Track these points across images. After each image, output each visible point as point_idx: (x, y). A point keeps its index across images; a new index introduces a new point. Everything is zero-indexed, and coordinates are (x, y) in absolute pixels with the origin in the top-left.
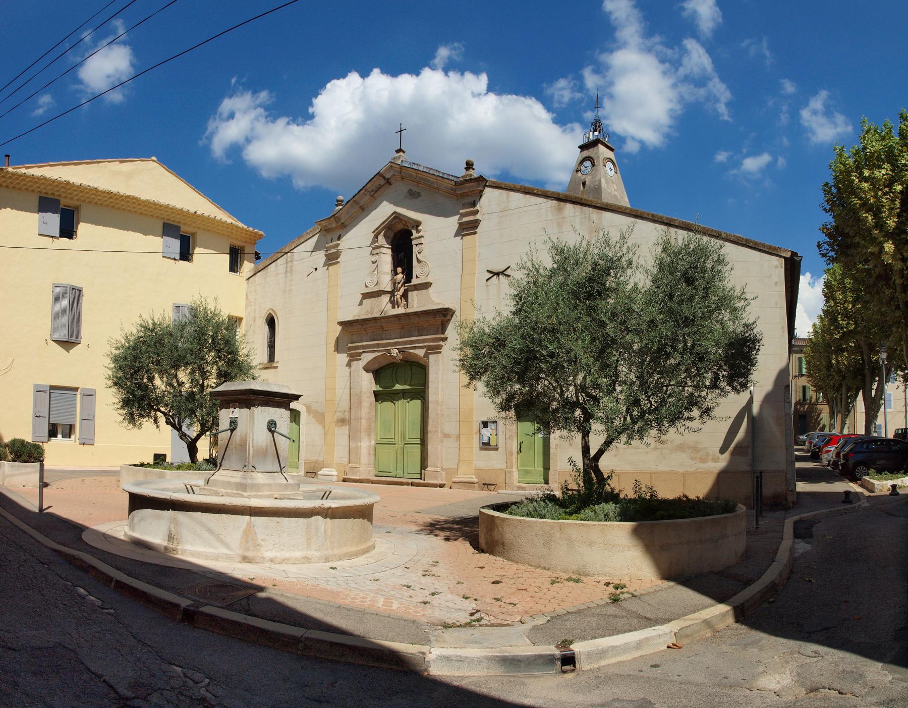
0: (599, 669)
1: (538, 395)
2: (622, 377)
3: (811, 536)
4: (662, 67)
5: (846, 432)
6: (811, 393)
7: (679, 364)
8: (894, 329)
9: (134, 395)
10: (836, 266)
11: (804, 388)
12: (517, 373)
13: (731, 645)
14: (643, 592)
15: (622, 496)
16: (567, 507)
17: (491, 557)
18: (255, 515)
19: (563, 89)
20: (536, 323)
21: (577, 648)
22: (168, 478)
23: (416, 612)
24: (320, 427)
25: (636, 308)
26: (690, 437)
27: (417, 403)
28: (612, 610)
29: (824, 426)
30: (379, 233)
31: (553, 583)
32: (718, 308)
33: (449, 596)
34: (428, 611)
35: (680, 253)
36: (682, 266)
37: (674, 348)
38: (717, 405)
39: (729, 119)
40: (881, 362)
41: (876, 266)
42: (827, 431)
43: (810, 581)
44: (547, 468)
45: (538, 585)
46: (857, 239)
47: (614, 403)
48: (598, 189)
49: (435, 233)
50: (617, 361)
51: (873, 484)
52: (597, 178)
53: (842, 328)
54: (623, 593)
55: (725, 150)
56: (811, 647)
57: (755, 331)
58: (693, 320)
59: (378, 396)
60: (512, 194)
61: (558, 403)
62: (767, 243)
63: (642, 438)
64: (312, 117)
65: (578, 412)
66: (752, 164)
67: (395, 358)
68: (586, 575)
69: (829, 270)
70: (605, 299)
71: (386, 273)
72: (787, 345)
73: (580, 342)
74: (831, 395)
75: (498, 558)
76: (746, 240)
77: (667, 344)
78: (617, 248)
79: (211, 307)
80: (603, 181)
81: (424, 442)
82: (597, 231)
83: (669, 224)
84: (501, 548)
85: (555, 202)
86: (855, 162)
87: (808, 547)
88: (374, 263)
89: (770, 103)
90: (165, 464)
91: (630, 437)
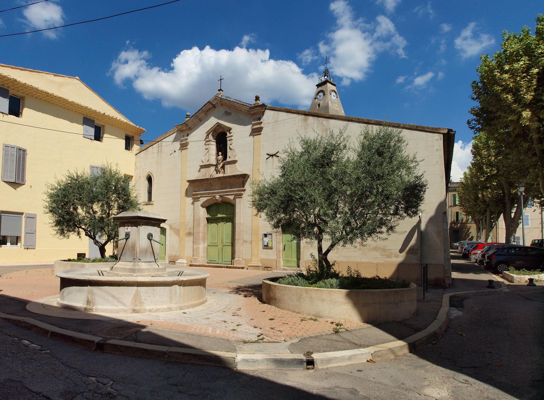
0: (327, 369)
1: (294, 220)
2: (341, 210)
3: (462, 306)
4: (364, 35)
5: (489, 241)
6: (463, 216)
7: (374, 201)
8: (531, 170)
9: (64, 218)
10: (482, 134)
11: (457, 213)
12: (282, 208)
13: (406, 365)
14: (353, 329)
15: (340, 275)
16: (310, 280)
17: (269, 306)
18: (140, 286)
19: (307, 55)
20: (293, 181)
21: (315, 356)
22: (87, 267)
23: (229, 335)
24: (177, 237)
25: (348, 171)
26: (380, 243)
27: (229, 224)
28: (335, 337)
29: (472, 237)
30: (209, 134)
31: (302, 320)
32: (398, 168)
33: (247, 326)
34: (235, 334)
35: (374, 138)
36: (376, 146)
37: (371, 193)
38: (398, 225)
39: (406, 57)
40: (519, 194)
41: (515, 129)
42: (474, 240)
43: (462, 335)
44: (298, 259)
45: (294, 321)
46: (499, 113)
47: (336, 224)
48: (327, 108)
49: (239, 134)
50: (338, 201)
51: (513, 277)
52: (326, 102)
53: (487, 173)
54: (341, 328)
55: (403, 76)
56: (463, 377)
57: (422, 180)
58: (382, 176)
59: (209, 221)
60: (280, 113)
61: (305, 224)
62: (431, 126)
63: (352, 243)
64: (173, 69)
65: (316, 229)
66: (420, 81)
67: (217, 200)
68: (321, 317)
69: (476, 137)
70: (331, 167)
71: (213, 155)
72: (445, 187)
73: (317, 191)
74: (477, 217)
75: (272, 307)
76: (417, 126)
77: (366, 190)
78: (338, 139)
79: (114, 169)
80: (330, 103)
81: (233, 244)
82: (326, 130)
83: (368, 123)
84: (274, 301)
85: (303, 116)
86: (497, 63)
87: (460, 313)
88: (206, 149)
89: (433, 41)
90: (85, 259)
91: (345, 243)
